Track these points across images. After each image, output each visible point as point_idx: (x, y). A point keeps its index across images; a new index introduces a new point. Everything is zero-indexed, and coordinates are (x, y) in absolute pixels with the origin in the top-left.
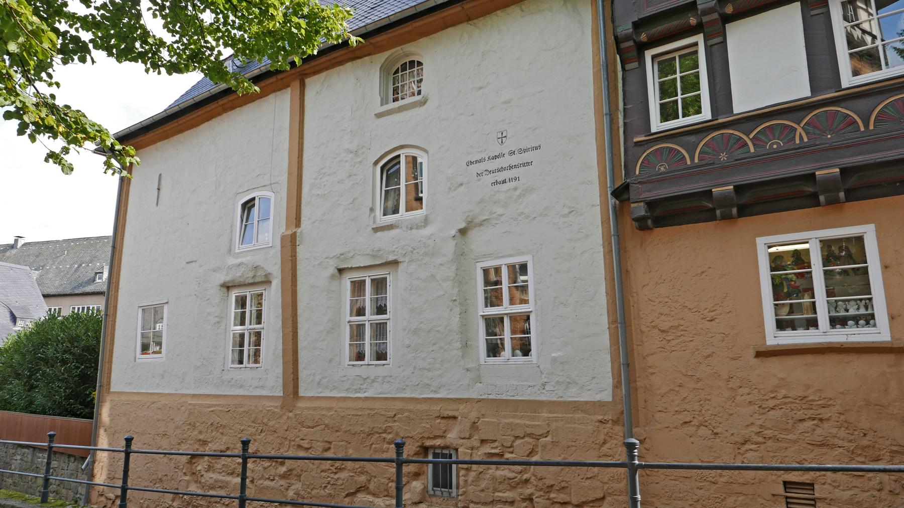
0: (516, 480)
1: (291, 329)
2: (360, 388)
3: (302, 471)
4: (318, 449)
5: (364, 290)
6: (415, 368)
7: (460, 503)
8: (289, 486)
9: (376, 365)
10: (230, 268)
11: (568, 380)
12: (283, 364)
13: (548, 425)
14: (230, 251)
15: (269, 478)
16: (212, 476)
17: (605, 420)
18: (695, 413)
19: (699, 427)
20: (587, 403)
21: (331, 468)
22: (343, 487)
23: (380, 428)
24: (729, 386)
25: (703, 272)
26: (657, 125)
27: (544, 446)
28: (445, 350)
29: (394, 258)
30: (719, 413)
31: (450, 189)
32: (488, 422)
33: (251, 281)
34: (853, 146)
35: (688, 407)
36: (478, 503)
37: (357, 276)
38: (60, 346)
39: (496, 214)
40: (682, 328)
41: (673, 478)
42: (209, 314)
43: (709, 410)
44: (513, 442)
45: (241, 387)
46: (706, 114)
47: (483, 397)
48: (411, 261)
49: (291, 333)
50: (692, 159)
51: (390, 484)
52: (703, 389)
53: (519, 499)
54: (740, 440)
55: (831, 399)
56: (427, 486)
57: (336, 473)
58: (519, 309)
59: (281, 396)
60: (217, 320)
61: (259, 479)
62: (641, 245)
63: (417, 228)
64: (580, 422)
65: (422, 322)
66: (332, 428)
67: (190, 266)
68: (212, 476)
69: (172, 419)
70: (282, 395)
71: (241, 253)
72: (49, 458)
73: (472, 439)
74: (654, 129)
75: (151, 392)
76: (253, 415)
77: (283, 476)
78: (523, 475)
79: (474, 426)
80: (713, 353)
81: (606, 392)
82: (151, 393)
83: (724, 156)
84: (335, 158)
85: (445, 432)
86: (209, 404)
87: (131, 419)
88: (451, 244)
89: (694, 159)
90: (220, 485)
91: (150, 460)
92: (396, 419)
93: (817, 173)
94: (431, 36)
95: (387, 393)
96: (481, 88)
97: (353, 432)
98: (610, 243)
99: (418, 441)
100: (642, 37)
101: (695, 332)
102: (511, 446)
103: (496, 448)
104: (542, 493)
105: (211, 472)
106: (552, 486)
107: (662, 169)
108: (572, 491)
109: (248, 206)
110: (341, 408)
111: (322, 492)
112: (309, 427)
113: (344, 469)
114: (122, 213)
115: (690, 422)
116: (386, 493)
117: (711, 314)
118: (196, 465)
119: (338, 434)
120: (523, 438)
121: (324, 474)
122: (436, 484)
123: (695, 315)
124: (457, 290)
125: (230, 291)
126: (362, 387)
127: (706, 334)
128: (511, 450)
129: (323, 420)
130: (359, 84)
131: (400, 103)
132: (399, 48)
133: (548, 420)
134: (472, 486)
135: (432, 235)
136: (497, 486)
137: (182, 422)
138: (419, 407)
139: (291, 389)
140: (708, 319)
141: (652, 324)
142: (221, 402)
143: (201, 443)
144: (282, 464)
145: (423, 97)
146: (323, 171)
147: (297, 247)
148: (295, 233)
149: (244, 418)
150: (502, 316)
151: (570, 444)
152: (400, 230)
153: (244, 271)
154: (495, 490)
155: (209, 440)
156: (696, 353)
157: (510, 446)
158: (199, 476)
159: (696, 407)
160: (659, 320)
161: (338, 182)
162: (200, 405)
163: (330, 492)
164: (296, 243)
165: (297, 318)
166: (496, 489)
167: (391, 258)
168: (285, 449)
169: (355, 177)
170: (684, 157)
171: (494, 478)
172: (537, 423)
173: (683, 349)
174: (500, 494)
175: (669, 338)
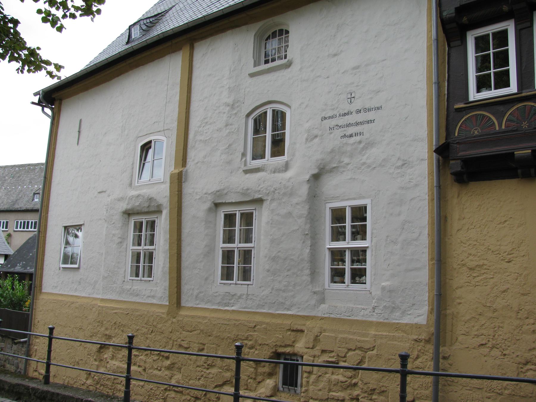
0: (346, 383)
2: (229, 303)
3: (182, 365)
4: (195, 349)
5: (63, 253)
6: (272, 289)
7: (302, 398)
8: (172, 376)
11: (394, 306)
12: (169, 279)
14: (131, 185)
15: (157, 369)
16: (115, 363)
17: (420, 339)
18: (490, 337)
19: (492, 348)
20: (406, 324)
21: (204, 364)
23: (243, 336)
24: (519, 317)
25: (506, 221)
26: (474, 95)
27: (370, 358)
28: (297, 276)
29: (260, 196)
30: (509, 338)
32: (328, 336)
33: (146, 210)
35: (484, 332)
36: (316, 400)
37: (230, 210)
39: (344, 163)
40: (485, 267)
41: (468, 388)
43: (501, 335)
44: (347, 353)
45: (137, 295)
46: (513, 88)
47: (326, 316)
48: (273, 200)
49: (176, 255)
50: (500, 125)
51: (249, 381)
52: (497, 318)
53: (348, 398)
54: (523, 361)
56: (278, 384)
57: (208, 369)
58: (359, 244)
59: (167, 305)
60: (120, 240)
61: (150, 369)
62: (458, 196)
63: (279, 172)
64: (400, 340)
65: (279, 252)
66: (206, 333)
67: (100, 195)
68: (115, 363)
69: (86, 317)
70: (168, 304)
71: (140, 186)
73: (315, 349)
74: (471, 99)
75: (71, 294)
76: (146, 319)
77: (169, 368)
78: (352, 380)
79: (316, 339)
80: (508, 289)
81: (423, 317)
82: (72, 296)
83: (525, 125)
84: (215, 110)
85: (294, 342)
86: (113, 307)
87: (56, 315)
89: (501, 125)
90: (121, 370)
91: (71, 347)
92: (256, 329)
93: (515, 153)
95: (250, 308)
96: (335, 55)
98: (433, 193)
99: (272, 348)
100: (463, 20)
101: (495, 271)
102: (345, 357)
103: (333, 357)
104: (366, 395)
105: (114, 360)
106: (374, 390)
107: (476, 132)
108: (390, 394)
109: (146, 148)
110: (213, 318)
112: (188, 331)
114: (52, 150)
115: (486, 344)
116: (246, 387)
117: (509, 256)
118: (103, 353)
119: (210, 338)
120: (354, 350)
121: (198, 369)
122: (284, 383)
123: (497, 257)
124: (309, 226)
125: (130, 218)
126: (230, 302)
127: (504, 273)
128: (344, 359)
129: (199, 326)
130: (236, 48)
131: (271, 65)
133: (375, 337)
134: (312, 386)
135: (290, 178)
136: (332, 387)
137: (93, 320)
138: (274, 321)
139: (175, 300)
140: (506, 260)
141: (462, 262)
143: (107, 337)
144: (167, 358)
145: (288, 61)
146: (206, 121)
147: (183, 183)
149: (139, 320)
150: (344, 249)
151: (390, 357)
152: (265, 173)
153: (141, 202)
154: (330, 390)
155: (113, 335)
156: (495, 288)
157: (344, 356)
158: (106, 362)
160: (468, 259)
161: (217, 130)
162: (107, 308)
163: (203, 383)
164: (182, 181)
165: (181, 242)
166: (331, 389)
167: (257, 196)
168: (170, 347)
169: (231, 127)
170: (494, 123)
171: (329, 381)
173: (485, 284)
174: (334, 394)
175: (475, 275)
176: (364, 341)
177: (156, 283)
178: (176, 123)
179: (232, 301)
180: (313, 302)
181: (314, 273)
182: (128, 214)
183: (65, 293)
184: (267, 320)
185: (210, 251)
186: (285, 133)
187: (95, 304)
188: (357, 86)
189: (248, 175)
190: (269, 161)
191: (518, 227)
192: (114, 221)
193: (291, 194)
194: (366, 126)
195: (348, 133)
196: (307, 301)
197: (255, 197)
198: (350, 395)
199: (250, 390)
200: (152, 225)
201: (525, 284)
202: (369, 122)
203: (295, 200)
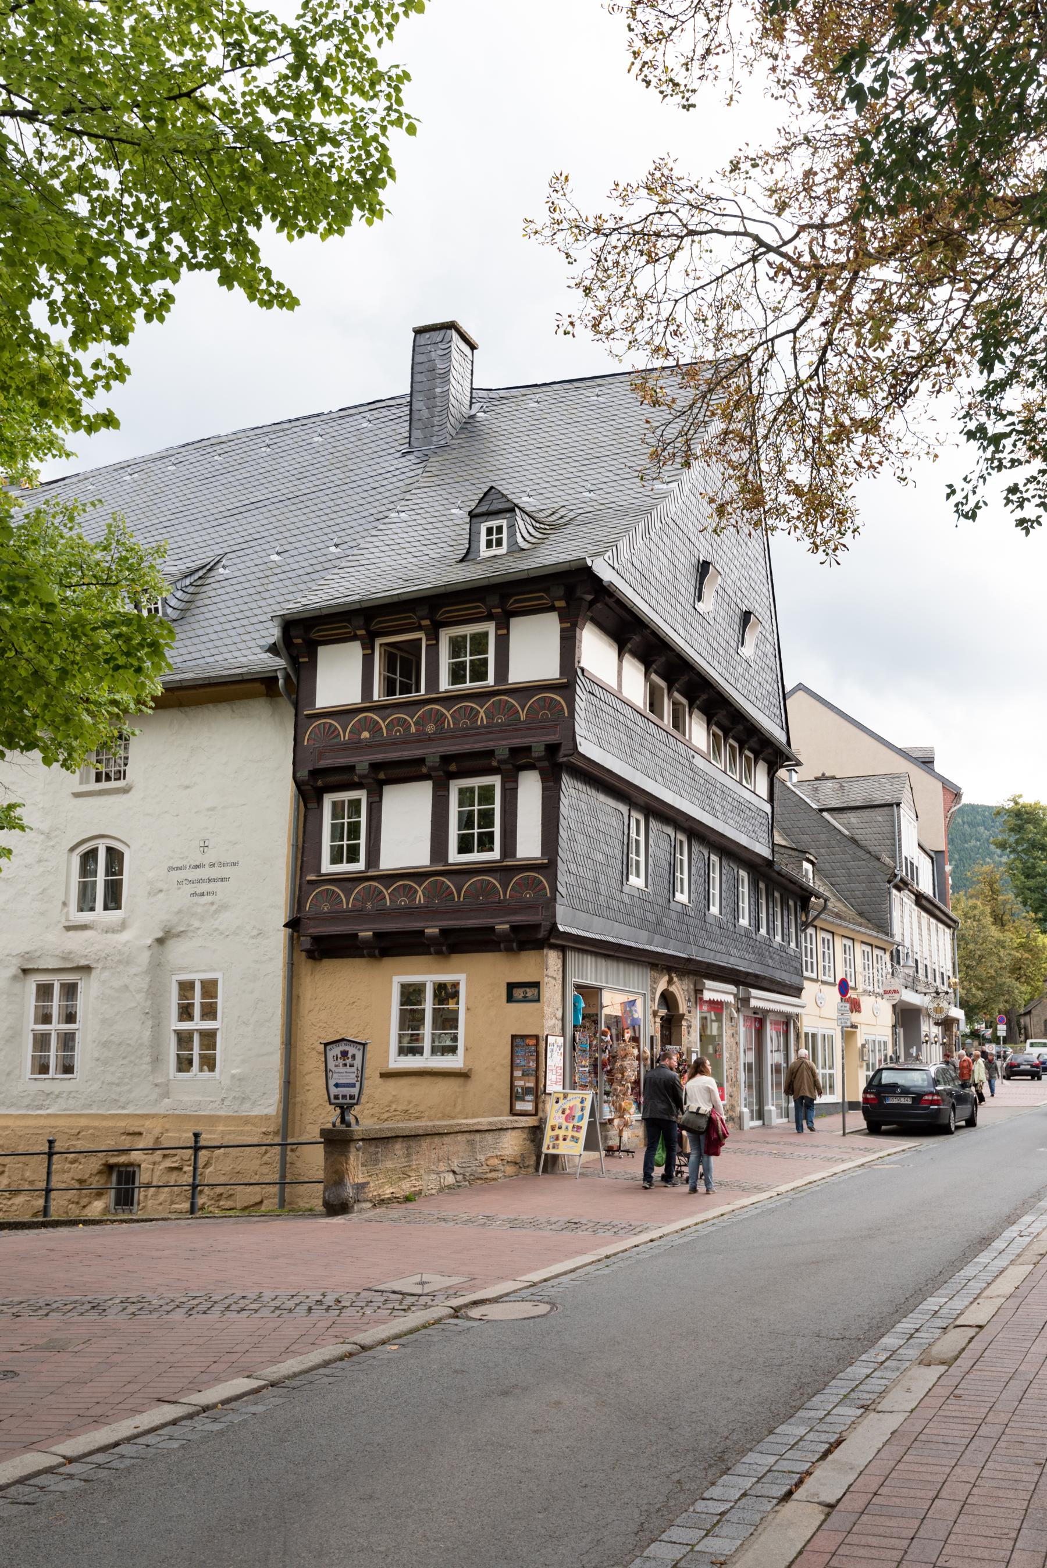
6: (103, 1083)
9: (62, 1079)
13: (222, 1138)
29: (87, 963)
31: (149, 893)
37: (44, 978)
47: (170, 1112)
48: (104, 968)
63: (113, 932)
74: (324, 871)
96: (187, 787)
135: (127, 942)
167: (83, 962)
179: (47, 1102)
181: (157, 1060)
184: (96, 1123)
190: (100, 915)
195: (199, 891)
196: (147, 1096)
202: (223, 880)
203: (133, 970)
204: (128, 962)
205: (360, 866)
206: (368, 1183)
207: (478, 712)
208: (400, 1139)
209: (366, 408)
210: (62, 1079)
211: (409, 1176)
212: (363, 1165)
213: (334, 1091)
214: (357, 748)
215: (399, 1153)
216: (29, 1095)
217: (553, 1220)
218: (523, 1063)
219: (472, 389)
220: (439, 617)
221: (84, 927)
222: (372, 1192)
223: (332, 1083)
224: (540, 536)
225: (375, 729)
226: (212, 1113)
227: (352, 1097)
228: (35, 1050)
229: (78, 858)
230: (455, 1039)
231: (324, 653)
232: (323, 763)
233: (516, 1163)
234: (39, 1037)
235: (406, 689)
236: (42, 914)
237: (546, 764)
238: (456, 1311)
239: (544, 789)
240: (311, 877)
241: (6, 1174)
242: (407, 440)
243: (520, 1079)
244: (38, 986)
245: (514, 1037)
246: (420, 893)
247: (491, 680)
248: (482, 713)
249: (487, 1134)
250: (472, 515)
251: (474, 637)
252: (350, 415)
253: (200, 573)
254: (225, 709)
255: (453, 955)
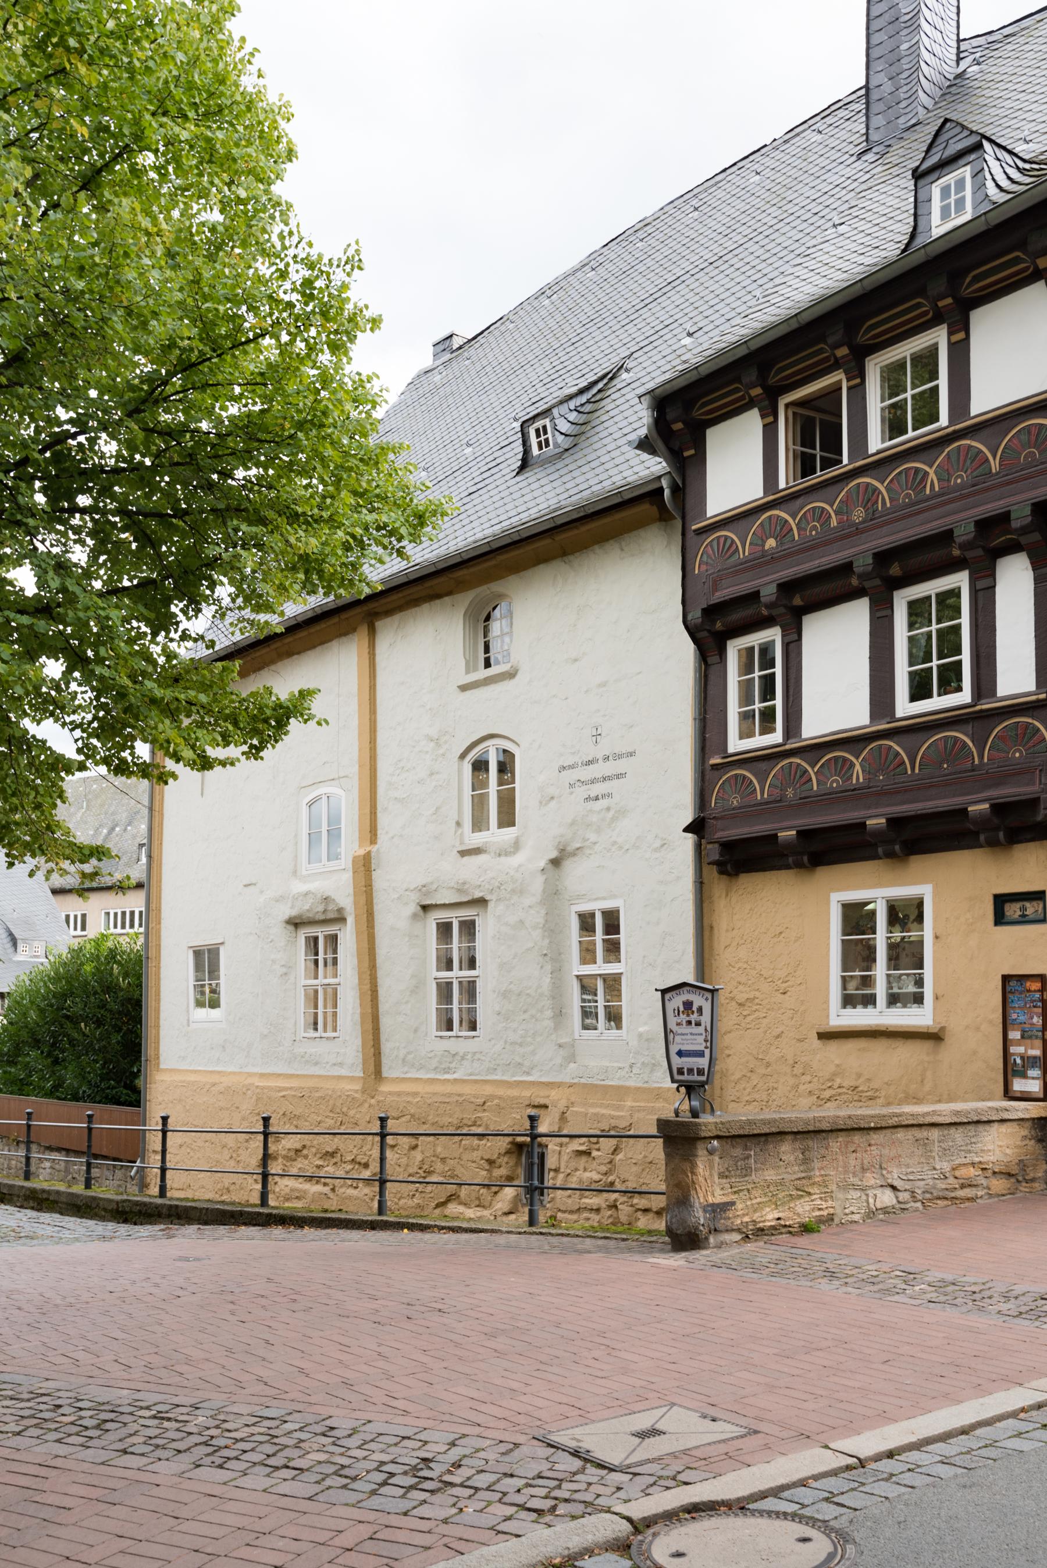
1: (368, 986)
5: (451, 937)
6: (506, 1042)
9: (466, 1038)
10: (295, 898)
13: (631, 1116)
14: (295, 873)
22: (432, 1195)
31: (541, 803)
33: (322, 917)
34: (911, 790)
35: (757, 1096)
37: (443, 915)
38: (92, 999)
42: (274, 961)
45: (316, 1064)
47: (575, 1081)
48: (499, 900)
49: (369, 992)
55: (877, 1090)
60: (284, 970)
62: (727, 895)
63: (506, 855)
65: (511, 983)
71: (309, 875)
72: (89, 1165)
74: (731, 749)
76: (331, 1102)
88: (540, 880)
93: (970, 809)
94: (522, 574)
96: (576, 660)
97: (441, 1124)
111: (410, 1203)
113: (433, 1172)
116: (477, 1203)
128: (597, 1146)
132: (485, 587)
135: (520, 866)
139: (372, 1068)
142: (294, 1083)
148: (369, 853)
159: (765, 1097)
162: (270, 1088)
167: (478, 894)
168: (369, 1147)
172: (621, 1114)
175: (745, 1013)
176: (618, 1117)
177: (345, 1042)
178: (357, 766)
179: (453, 1065)
180: (558, 1060)
181: (560, 1014)
182: (296, 923)
183: (200, 1068)
184: (501, 1092)
185: (416, 989)
186: (514, 788)
187: (250, 1084)
188: (604, 716)
189: (466, 858)
190: (495, 835)
191: (796, 941)
192: (272, 937)
193: (520, 891)
194: (615, 782)
196: (551, 1060)
197: (476, 897)
198: (607, 1200)
199: (484, 1207)
200: (333, 940)
201: (801, 1025)
202: (619, 776)
203: (528, 901)
204: (520, 891)
205: (776, 737)
206: (733, 1203)
207: (926, 474)
208: (790, 1137)
209: (818, 118)
210: (466, 1038)
211: (809, 1194)
212: (722, 1176)
213: (677, 1061)
214: (760, 565)
215: (789, 1157)
216: (436, 1055)
217: (1019, 1289)
218: (1022, 1018)
219: (959, 41)
220: (862, 338)
221: (476, 851)
222: (741, 1214)
223: (674, 1049)
224: (1029, 180)
225: (782, 531)
226: (621, 1083)
227: (700, 1072)
228: (439, 1003)
229: (470, 766)
230: (920, 982)
231: (715, 437)
232: (720, 596)
233: (1010, 1175)
234: (465, 985)
235: (827, 464)
236: (436, 838)
237: (1036, 537)
238: (637, 1531)
239: (1037, 581)
240: (716, 760)
241: (420, 1148)
242: (864, 138)
243: (1018, 1043)
244: (438, 924)
245: (1006, 979)
246: (858, 767)
247: (944, 420)
248: (932, 476)
249: (953, 1130)
250: (918, 175)
251: (916, 359)
252: (798, 135)
253: (600, 385)
254: (613, 547)
255: (913, 858)
